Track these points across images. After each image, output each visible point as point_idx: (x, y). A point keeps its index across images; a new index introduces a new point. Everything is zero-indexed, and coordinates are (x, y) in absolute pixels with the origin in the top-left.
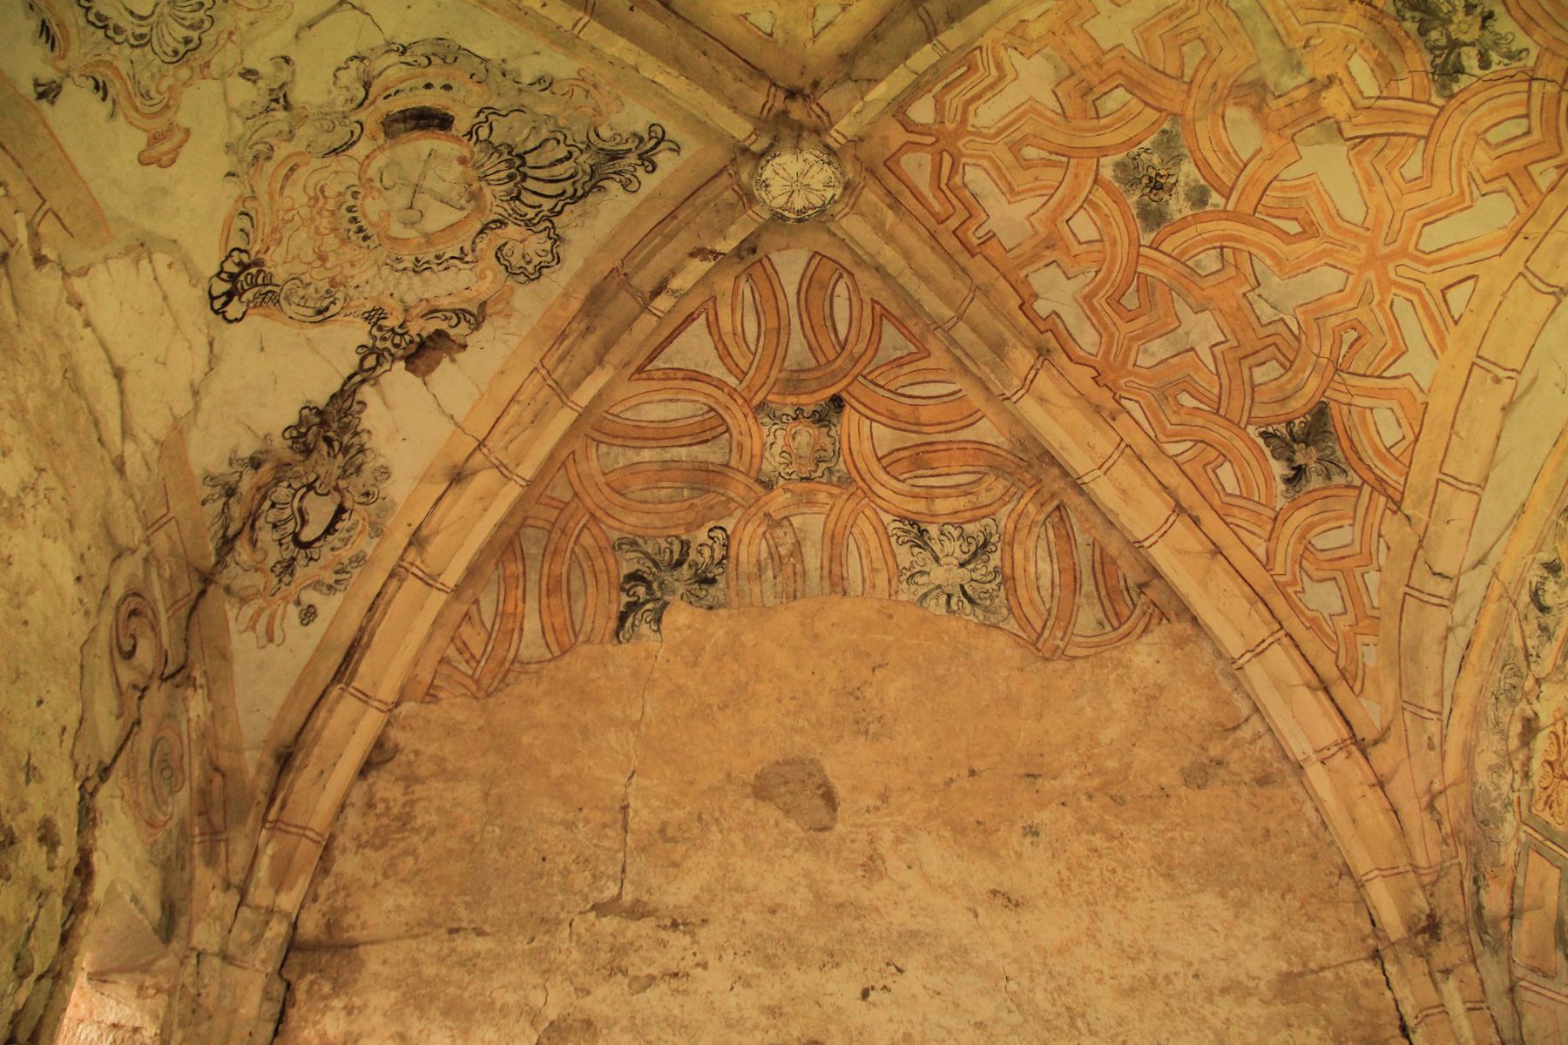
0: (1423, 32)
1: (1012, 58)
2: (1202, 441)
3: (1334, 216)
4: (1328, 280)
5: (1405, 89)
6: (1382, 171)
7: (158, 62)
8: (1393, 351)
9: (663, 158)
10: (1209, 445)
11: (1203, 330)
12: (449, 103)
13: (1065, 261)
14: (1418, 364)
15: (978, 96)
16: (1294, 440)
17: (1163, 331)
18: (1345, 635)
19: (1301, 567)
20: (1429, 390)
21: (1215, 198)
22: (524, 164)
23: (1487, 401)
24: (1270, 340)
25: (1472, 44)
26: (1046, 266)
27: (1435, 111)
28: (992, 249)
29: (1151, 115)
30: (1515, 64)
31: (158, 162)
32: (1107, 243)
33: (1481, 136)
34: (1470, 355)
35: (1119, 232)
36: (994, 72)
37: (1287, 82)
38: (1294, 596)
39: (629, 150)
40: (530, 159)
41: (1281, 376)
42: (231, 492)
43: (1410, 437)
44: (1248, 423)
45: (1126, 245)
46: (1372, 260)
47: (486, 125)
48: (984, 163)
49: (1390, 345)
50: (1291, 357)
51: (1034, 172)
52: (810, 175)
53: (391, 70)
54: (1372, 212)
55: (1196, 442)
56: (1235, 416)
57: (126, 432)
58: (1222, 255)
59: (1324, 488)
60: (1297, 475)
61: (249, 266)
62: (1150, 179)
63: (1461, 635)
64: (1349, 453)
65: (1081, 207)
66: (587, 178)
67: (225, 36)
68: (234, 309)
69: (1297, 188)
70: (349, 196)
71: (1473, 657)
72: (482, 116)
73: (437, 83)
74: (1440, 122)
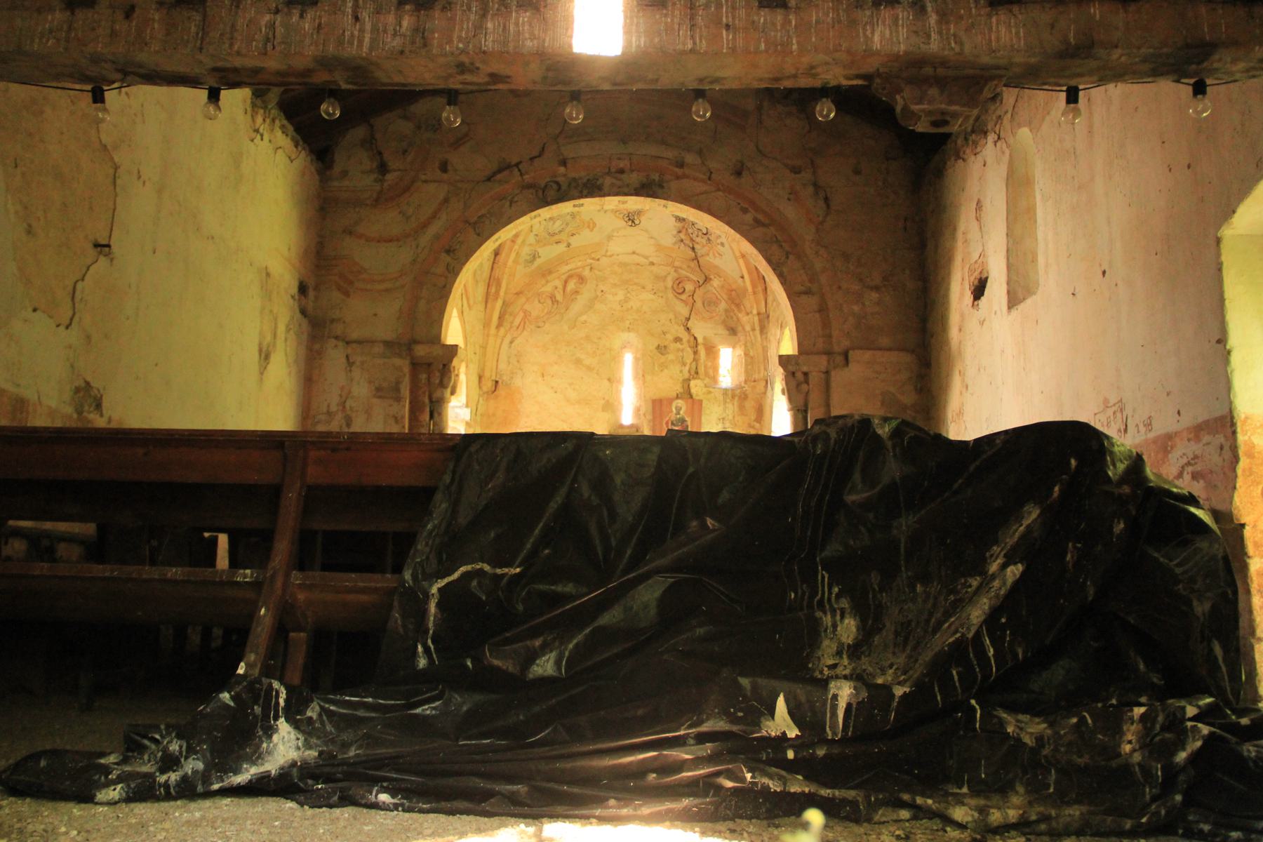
31: (594, 227)
42: (682, 241)
57: (646, 258)
68: (637, 222)
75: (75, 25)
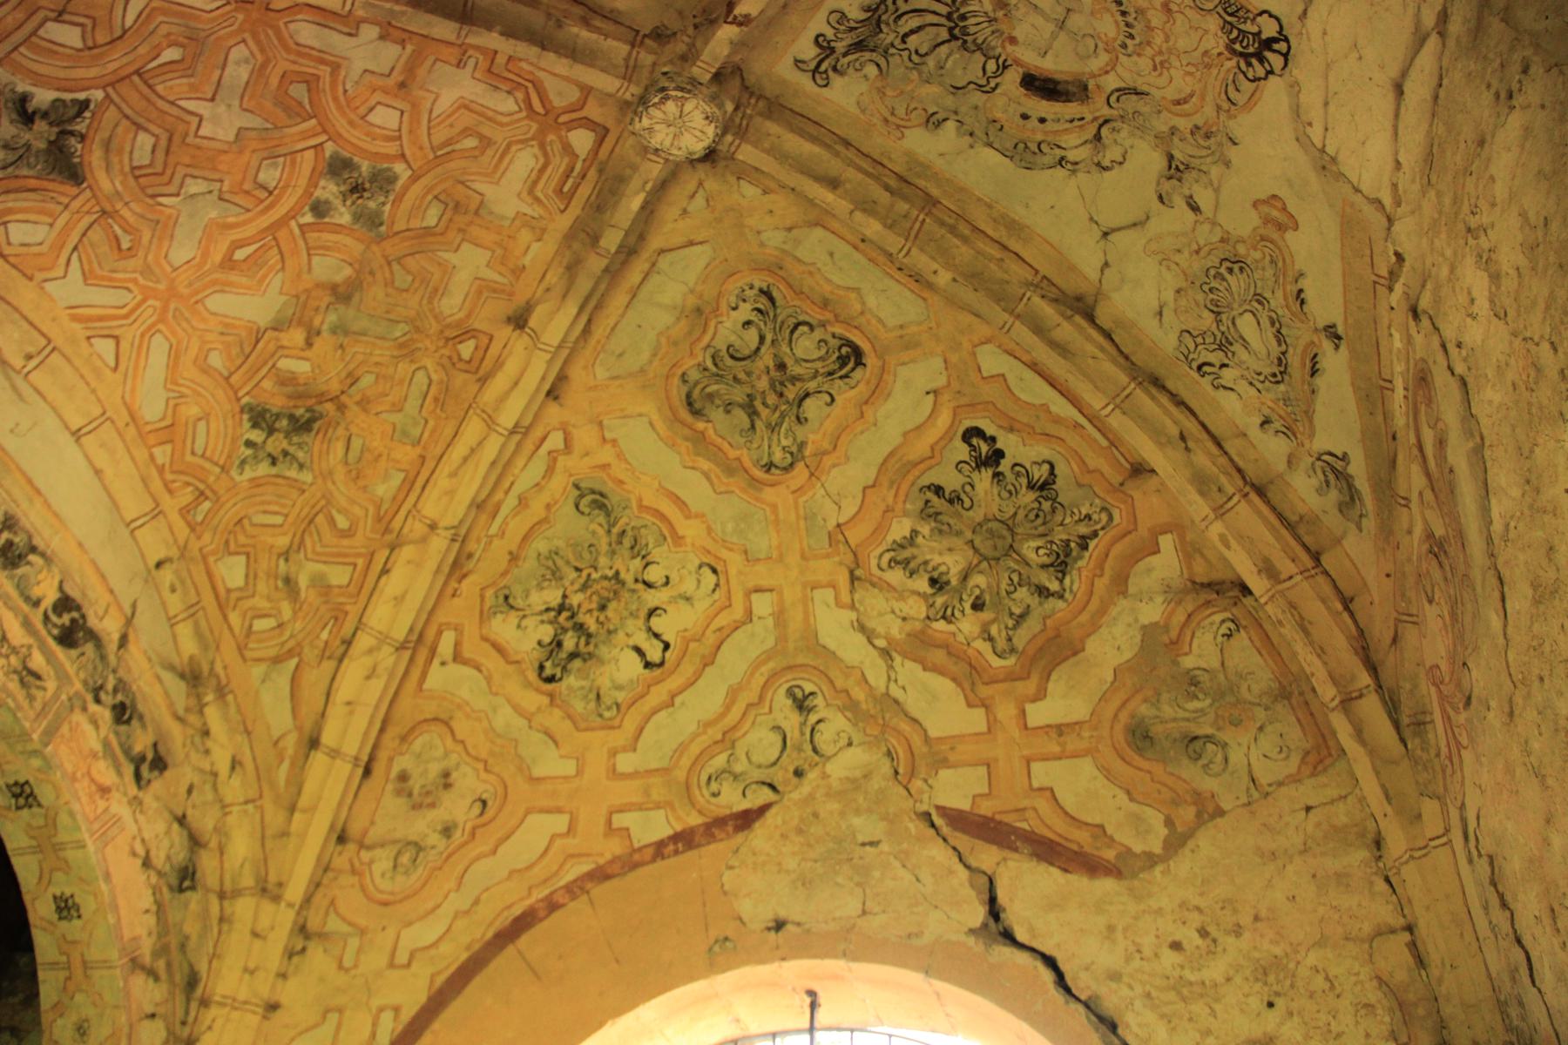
0: (292, 417)
2: (120, 37)
3: (223, 287)
4: (182, 251)
5: (267, 384)
7: (1256, 276)
8: (92, 271)
9: (810, 52)
12: (1023, 100)
13: (380, 82)
14: (69, 289)
16: (63, 133)
21: (308, 218)
22: (951, 30)
24: (169, 172)
26: (392, 69)
28: (451, 54)
33: (206, 417)
34: (59, 341)
35: (355, 136)
36: (540, 195)
37: (332, 318)
39: (845, 55)
40: (945, 35)
41: (131, 160)
44: (107, 96)
45: (342, 131)
46: (172, 292)
47: (989, 74)
48: (505, 120)
49: (99, 272)
50: (142, 180)
51: (457, 130)
53: (1075, 144)
54: (205, 314)
55: (125, 32)
56: (124, 88)
58: (265, 188)
60: (24, 113)
61: (1241, 54)
66: (884, 18)
67: (1202, 253)
68: (1270, 30)
69: (265, 277)
70: (1130, 49)
72: (992, 85)
73: (1034, 123)
74: (231, 393)
75: (1443, 990)
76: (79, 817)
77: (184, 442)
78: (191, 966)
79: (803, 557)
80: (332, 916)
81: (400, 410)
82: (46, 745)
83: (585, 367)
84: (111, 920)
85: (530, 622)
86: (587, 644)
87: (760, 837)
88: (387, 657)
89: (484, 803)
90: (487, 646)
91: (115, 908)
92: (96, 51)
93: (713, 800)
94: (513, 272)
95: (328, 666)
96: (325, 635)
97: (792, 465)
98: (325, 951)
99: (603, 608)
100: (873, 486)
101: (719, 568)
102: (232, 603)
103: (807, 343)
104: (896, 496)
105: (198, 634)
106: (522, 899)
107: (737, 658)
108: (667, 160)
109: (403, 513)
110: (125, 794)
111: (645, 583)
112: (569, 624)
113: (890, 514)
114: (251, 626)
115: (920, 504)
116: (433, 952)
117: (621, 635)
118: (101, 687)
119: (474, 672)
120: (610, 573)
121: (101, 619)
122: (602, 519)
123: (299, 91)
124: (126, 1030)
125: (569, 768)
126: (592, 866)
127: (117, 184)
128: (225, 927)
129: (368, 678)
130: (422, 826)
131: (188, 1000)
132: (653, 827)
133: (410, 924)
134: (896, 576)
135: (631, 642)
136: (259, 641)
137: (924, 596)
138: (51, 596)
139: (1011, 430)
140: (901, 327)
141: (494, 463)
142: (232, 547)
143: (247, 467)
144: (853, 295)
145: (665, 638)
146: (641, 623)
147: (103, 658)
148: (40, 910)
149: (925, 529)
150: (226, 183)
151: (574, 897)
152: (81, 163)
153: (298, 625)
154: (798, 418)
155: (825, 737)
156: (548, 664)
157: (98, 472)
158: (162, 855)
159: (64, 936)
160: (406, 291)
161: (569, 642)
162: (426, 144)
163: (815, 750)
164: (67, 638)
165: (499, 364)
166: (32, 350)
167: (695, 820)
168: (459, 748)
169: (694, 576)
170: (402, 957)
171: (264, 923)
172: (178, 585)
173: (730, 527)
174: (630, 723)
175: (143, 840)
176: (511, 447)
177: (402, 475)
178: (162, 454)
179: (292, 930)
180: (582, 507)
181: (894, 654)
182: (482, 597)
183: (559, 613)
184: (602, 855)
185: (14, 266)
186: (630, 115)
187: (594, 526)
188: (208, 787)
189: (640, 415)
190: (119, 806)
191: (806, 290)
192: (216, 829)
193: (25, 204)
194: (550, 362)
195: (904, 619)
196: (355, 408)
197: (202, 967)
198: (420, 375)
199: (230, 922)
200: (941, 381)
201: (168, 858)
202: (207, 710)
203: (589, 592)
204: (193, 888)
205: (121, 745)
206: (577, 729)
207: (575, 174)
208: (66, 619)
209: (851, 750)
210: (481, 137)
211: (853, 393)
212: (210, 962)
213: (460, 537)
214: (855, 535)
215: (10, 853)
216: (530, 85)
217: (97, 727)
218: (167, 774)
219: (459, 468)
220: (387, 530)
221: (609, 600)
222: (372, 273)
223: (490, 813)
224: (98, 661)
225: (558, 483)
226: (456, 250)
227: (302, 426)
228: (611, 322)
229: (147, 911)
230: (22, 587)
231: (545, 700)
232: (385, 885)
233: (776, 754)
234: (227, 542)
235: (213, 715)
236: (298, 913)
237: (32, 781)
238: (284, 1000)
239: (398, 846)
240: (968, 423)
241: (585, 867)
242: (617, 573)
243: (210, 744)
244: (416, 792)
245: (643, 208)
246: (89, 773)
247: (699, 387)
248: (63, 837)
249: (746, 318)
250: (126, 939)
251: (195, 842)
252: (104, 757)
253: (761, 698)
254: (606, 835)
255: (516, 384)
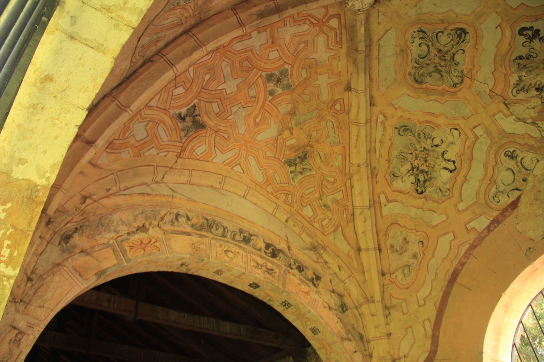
0: (299, 157)
1: (332, 53)
4: (242, 130)
5: (287, 152)
6: (269, 146)
10: (192, 83)
11: (231, 87)
14: (220, 158)
15: (328, 40)
16: (194, 117)
17: (233, 73)
18: (128, 142)
19: (150, 121)
20: (213, 162)
21: (270, 98)
23: (214, 181)
24: (226, 110)
25: (296, 169)
26: (267, 39)
27: (281, 160)
29: (296, 84)
30: (291, 179)
32: (266, 61)
33: (275, 171)
34: (225, 174)
38: (136, 118)
43: (199, 157)
44: (199, 100)
49: (224, 148)
50: (220, 116)
52: (361, 3)
55: (193, 79)
56: (201, 95)
58: (253, 97)
59: (179, 129)
60: (182, 119)
62: (281, 79)
63: (149, 190)
64: (192, 137)
65: (280, 56)
69: (268, 123)
71: (147, 198)
74: (278, 161)
76: (304, 304)
77: (274, 182)
78: (359, 333)
79: (484, 108)
80: (393, 299)
81: (329, 137)
82: (285, 288)
83: (377, 90)
84: (329, 329)
85: (405, 178)
86: (427, 175)
87: (522, 208)
88: (367, 213)
89: (422, 242)
90: (395, 193)
91: (328, 325)
92: (189, 90)
93: (498, 204)
94: (338, 75)
95: (351, 224)
96: (345, 216)
97: (462, 80)
98: (396, 311)
99: (426, 161)
100: (495, 70)
101: (457, 128)
102: (313, 221)
103: (444, 38)
104: (505, 69)
105: (309, 235)
106: (451, 267)
107: (480, 153)
108: (364, 11)
109: (347, 167)
110: (314, 291)
111: (435, 146)
112: (418, 172)
113: (507, 76)
114: (322, 225)
115: (516, 66)
116: (431, 296)
117: (437, 166)
118: (290, 264)
119: (396, 203)
120: (422, 149)
121: (280, 245)
122: (410, 134)
123: (246, 64)
124: (350, 359)
125: (444, 217)
126: (469, 245)
127: (215, 121)
128: (362, 317)
129: (365, 222)
130: (406, 258)
131: (363, 343)
132: (483, 223)
133: (418, 291)
134: (522, 95)
135: (442, 167)
136: (327, 227)
137: (537, 96)
138: (263, 246)
139: (537, 20)
140: (474, 12)
141: (366, 136)
142: (304, 204)
143: (295, 179)
144: (450, 13)
145: (452, 160)
146: (441, 159)
147: (286, 255)
148: (308, 335)
149: (523, 73)
150: (242, 103)
151: (468, 258)
152: (203, 122)
153: (335, 217)
154: (455, 64)
155: (527, 163)
156: (418, 188)
157: (256, 204)
158: (333, 304)
159: (318, 339)
160: (310, 101)
161: (421, 178)
162: (290, 54)
163: (526, 169)
164: (274, 255)
165: (350, 105)
166: (220, 180)
167: (496, 214)
168: (405, 229)
169: (450, 135)
170: (422, 303)
171: (373, 311)
172: (296, 224)
173: (453, 112)
174: (456, 193)
175: (325, 302)
176: (369, 128)
177: (341, 155)
178: (269, 189)
179: (383, 309)
180: (401, 134)
181: (537, 122)
182: (386, 179)
183: (413, 171)
184: (470, 240)
185: (203, 161)
186: (344, 5)
187: (408, 137)
188: (335, 278)
189: (403, 94)
190: (315, 296)
191: (433, 21)
192: (344, 289)
193: (195, 143)
194: (365, 95)
195: (534, 108)
196: (316, 144)
197: (362, 332)
198: (329, 123)
199: (363, 314)
200: (499, 20)
201: (335, 304)
202: (323, 256)
203: (419, 159)
204: (347, 310)
205: (305, 278)
206: (440, 204)
207: (338, 34)
208: (270, 250)
209: (540, 162)
210: (304, 42)
211: (469, 44)
212: (364, 329)
213: (369, 164)
214: (498, 90)
215: (291, 322)
216: (308, 17)
217: (296, 276)
218: (322, 280)
219: (356, 143)
220: (346, 175)
221: (427, 158)
222: (297, 102)
223: (425, 244)
224: (285, 257)
225: (389, 130)
226: (317, 80)
227: (303, 158)
228: (377, 71)
229: (338, 322)
230: (254, 247)
231: (424, 200)
232: (404, 282)
233: (513, 177)
234: (302, 204)
235: (325, 256)
236: (382, 303)
237: (286, 300)
238: (391, 331)
239: (402, 268)
240: (518, 29)
241: (467, 247)
242: (424, 148)
243: (329, 265)
244: (398, 249)
245: (365, 30)
246: (300, 290)
247: (417, 74)
248: (303, 311)
249: (419, 43)
250: (336, 332)
251: (340, 296)
252: (302, 284)
253: (496, 162)
254: (468, 233)
255: (359, 108)
